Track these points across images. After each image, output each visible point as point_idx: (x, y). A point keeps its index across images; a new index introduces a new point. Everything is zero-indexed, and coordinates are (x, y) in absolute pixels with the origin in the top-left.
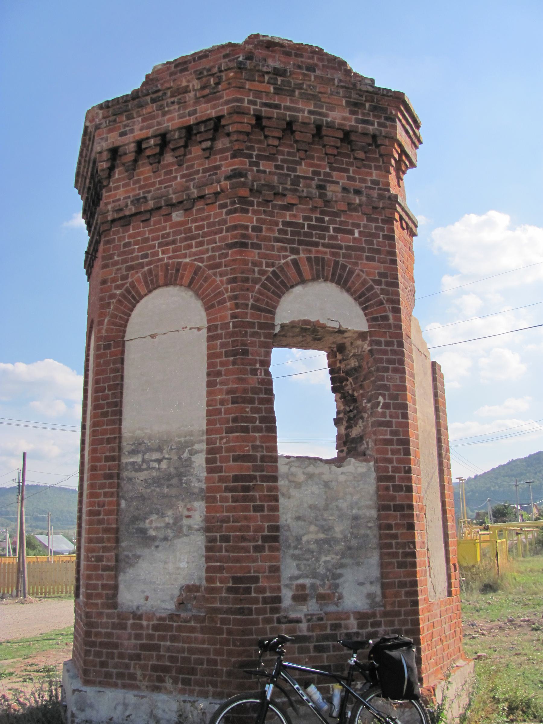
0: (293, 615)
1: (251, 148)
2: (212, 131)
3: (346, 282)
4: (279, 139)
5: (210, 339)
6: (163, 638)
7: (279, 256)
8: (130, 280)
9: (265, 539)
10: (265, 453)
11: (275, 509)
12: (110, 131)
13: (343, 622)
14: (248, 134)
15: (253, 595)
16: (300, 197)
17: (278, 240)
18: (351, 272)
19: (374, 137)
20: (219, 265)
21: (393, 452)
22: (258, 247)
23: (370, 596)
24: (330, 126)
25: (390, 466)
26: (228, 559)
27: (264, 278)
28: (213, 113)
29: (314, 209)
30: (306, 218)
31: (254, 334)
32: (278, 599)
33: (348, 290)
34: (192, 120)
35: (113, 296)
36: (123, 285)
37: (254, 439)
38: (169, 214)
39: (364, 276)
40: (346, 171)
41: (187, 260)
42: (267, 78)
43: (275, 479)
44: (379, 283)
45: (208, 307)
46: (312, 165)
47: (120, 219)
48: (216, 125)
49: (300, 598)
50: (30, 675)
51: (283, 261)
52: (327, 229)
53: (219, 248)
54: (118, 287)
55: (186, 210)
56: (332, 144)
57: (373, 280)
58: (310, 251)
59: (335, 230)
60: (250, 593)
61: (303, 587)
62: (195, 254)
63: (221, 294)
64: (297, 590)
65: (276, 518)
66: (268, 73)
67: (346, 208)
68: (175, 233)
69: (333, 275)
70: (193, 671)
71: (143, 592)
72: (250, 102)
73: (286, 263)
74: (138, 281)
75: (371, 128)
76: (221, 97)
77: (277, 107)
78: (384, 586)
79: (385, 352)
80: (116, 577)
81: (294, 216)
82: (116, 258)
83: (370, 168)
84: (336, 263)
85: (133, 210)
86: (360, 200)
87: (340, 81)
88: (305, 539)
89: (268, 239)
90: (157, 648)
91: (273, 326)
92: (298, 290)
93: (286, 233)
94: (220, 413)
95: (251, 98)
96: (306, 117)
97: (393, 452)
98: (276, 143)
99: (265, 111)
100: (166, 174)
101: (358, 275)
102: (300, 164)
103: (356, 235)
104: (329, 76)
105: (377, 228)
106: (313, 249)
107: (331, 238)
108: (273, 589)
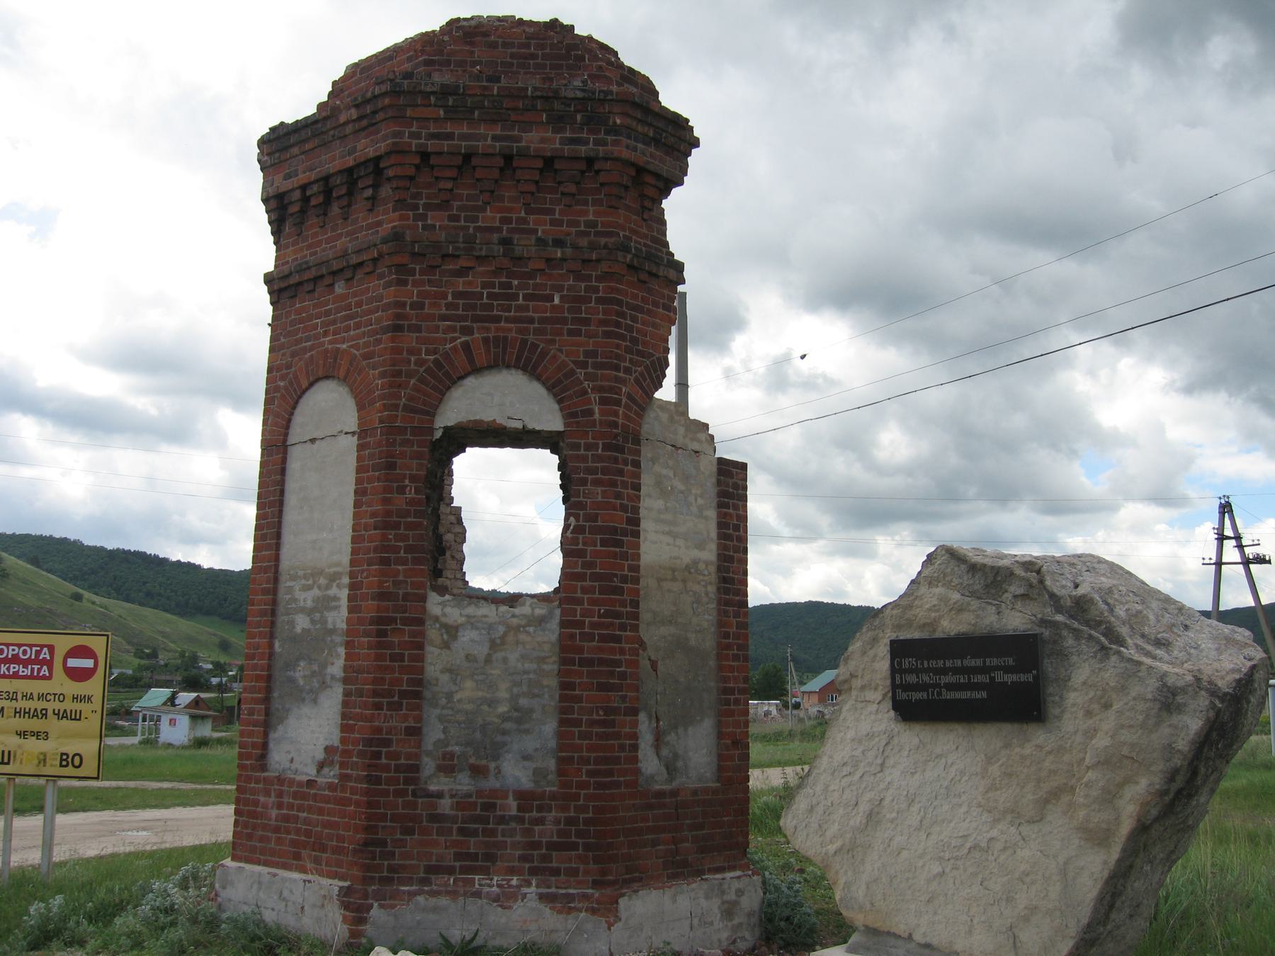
0: (433, 788)
1: (417, 196)
2: (372, 177)
3: (535, 368)
4: (454, 179)
7: (445, 339)
9: (403, 694)
10: (409, 590)
11: (421, 658)
13: (499, 802)
14: (412, 178)
15: (384, 761)
16: (478, 258)
17: (444, 318)
18: (544, 354)
19: (590, 161)
21: (584, 590)
22: (418, 329)
23: (538, 774)
24: (524, 154)
25: (579, 608)
27: (422, 370)
28: (371, 153)
29: (497, 272)
30: (484, 286)
31: (406, 442)
32: (416, 768)
33: (538, 379)
34: (350, 161)
36: (287, 374)
37: (397, 573)
38: (332, 285)
39: (563, 357)
40: (552, 212)
42: (433, 99)
43: (421, 622)
44: (583, 365)
45: (361, 407)
46: (501, 210)
47: (286, 288)
48: (375, 166)
49: (448, 766)
51: (448, 346)
52: (515, 297)
55: (348, 280)
56: (527, 177)
57: (575, 362)
58: (488, 330)
59: (526, 297)
60: (380, 758)
61: (452, 755)
64: (444, 758)
65: (421, 670)
66: (433, 93)
67: (542, 265)
69: (519, 358)
71: (288, 752)
72: (412, 135)
73: (454, 349)
75: (583, 148)
77: (450, 136)
78: (561, 761)
79: (584, 459)
80: (266, 735)
81: (470, 283)
83: (586, 203)
84: (524, 342)
86: (563, 253)
87: (535, 89)
88: (457, 697)
89: (431, 317)
91: (431, 430)
92: (470, 382)
93: (456, 307)
95: (414, 129)
96: (489, 146)
97: (584, 590)
98: (449, 185)
99: (431, 145)
101: (554, 357)
102: (485, 211)
103: (557, 301)
104: (520, 84)
105: (587, 289)
106: (492, 326)
107: (519, 308)
108: (409, 756)
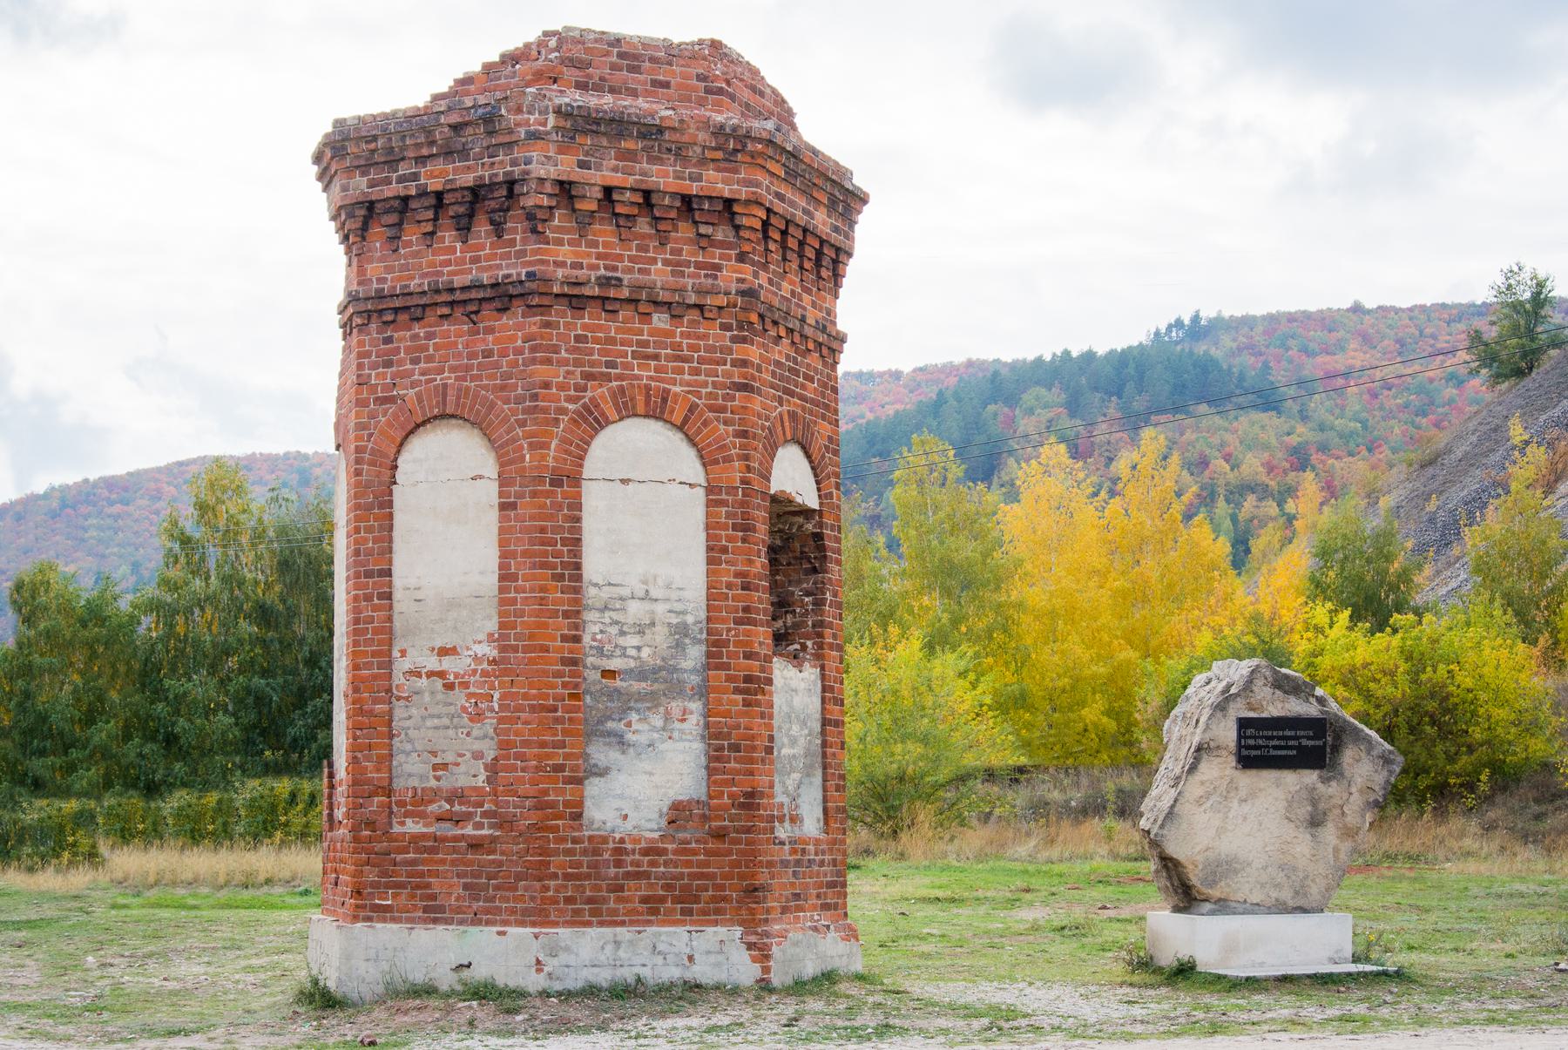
5: (710, 504)
6: (653, 864)
8: (589, 394)
12: (561, 151)
20: (723, 409)
26: (738, 772)
35: (563, 411)
41: (677, 389)
50: (428, 886)
53: (723, 386)
54: (569, 399)
55: (673, 316)
62: (688, 384)
63: (724, 448)
68: (658, 345)
70: (697, 900)
74: (602, 397)
76: (736, 171)
82: (564, 354)
85: (597, 291)
90: (647, 875)
94: (727, 599)
100: (639, 248)
